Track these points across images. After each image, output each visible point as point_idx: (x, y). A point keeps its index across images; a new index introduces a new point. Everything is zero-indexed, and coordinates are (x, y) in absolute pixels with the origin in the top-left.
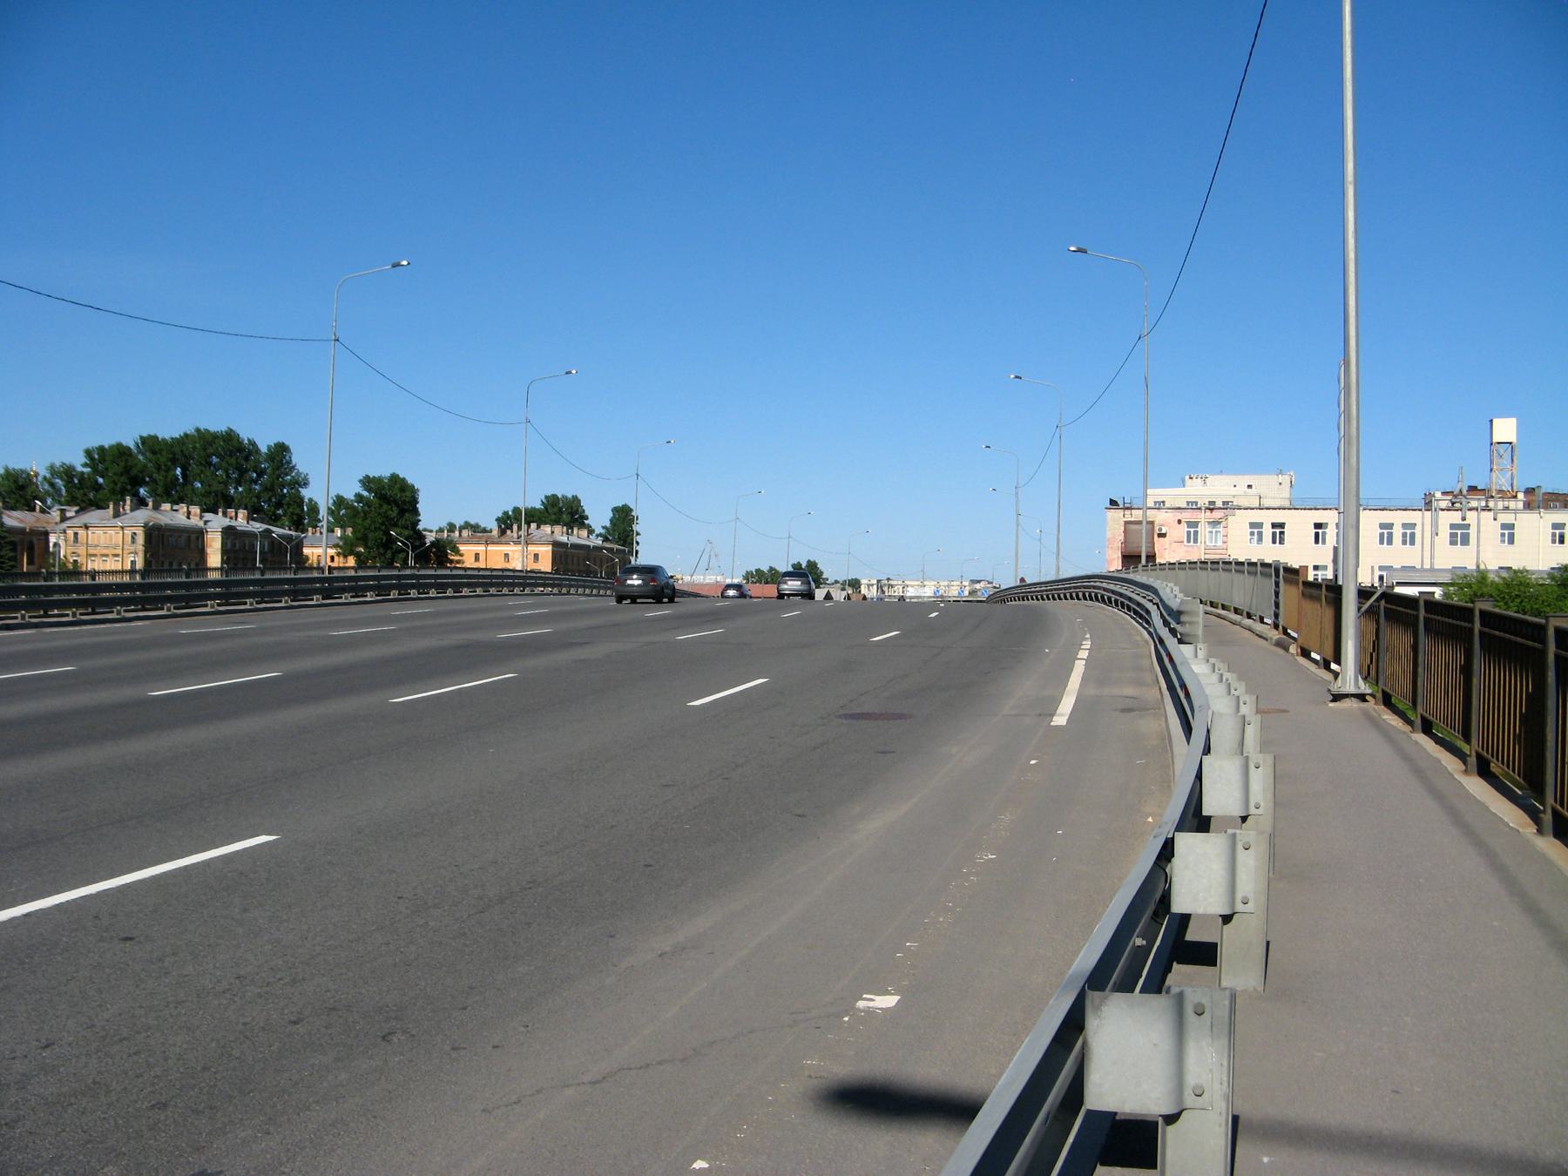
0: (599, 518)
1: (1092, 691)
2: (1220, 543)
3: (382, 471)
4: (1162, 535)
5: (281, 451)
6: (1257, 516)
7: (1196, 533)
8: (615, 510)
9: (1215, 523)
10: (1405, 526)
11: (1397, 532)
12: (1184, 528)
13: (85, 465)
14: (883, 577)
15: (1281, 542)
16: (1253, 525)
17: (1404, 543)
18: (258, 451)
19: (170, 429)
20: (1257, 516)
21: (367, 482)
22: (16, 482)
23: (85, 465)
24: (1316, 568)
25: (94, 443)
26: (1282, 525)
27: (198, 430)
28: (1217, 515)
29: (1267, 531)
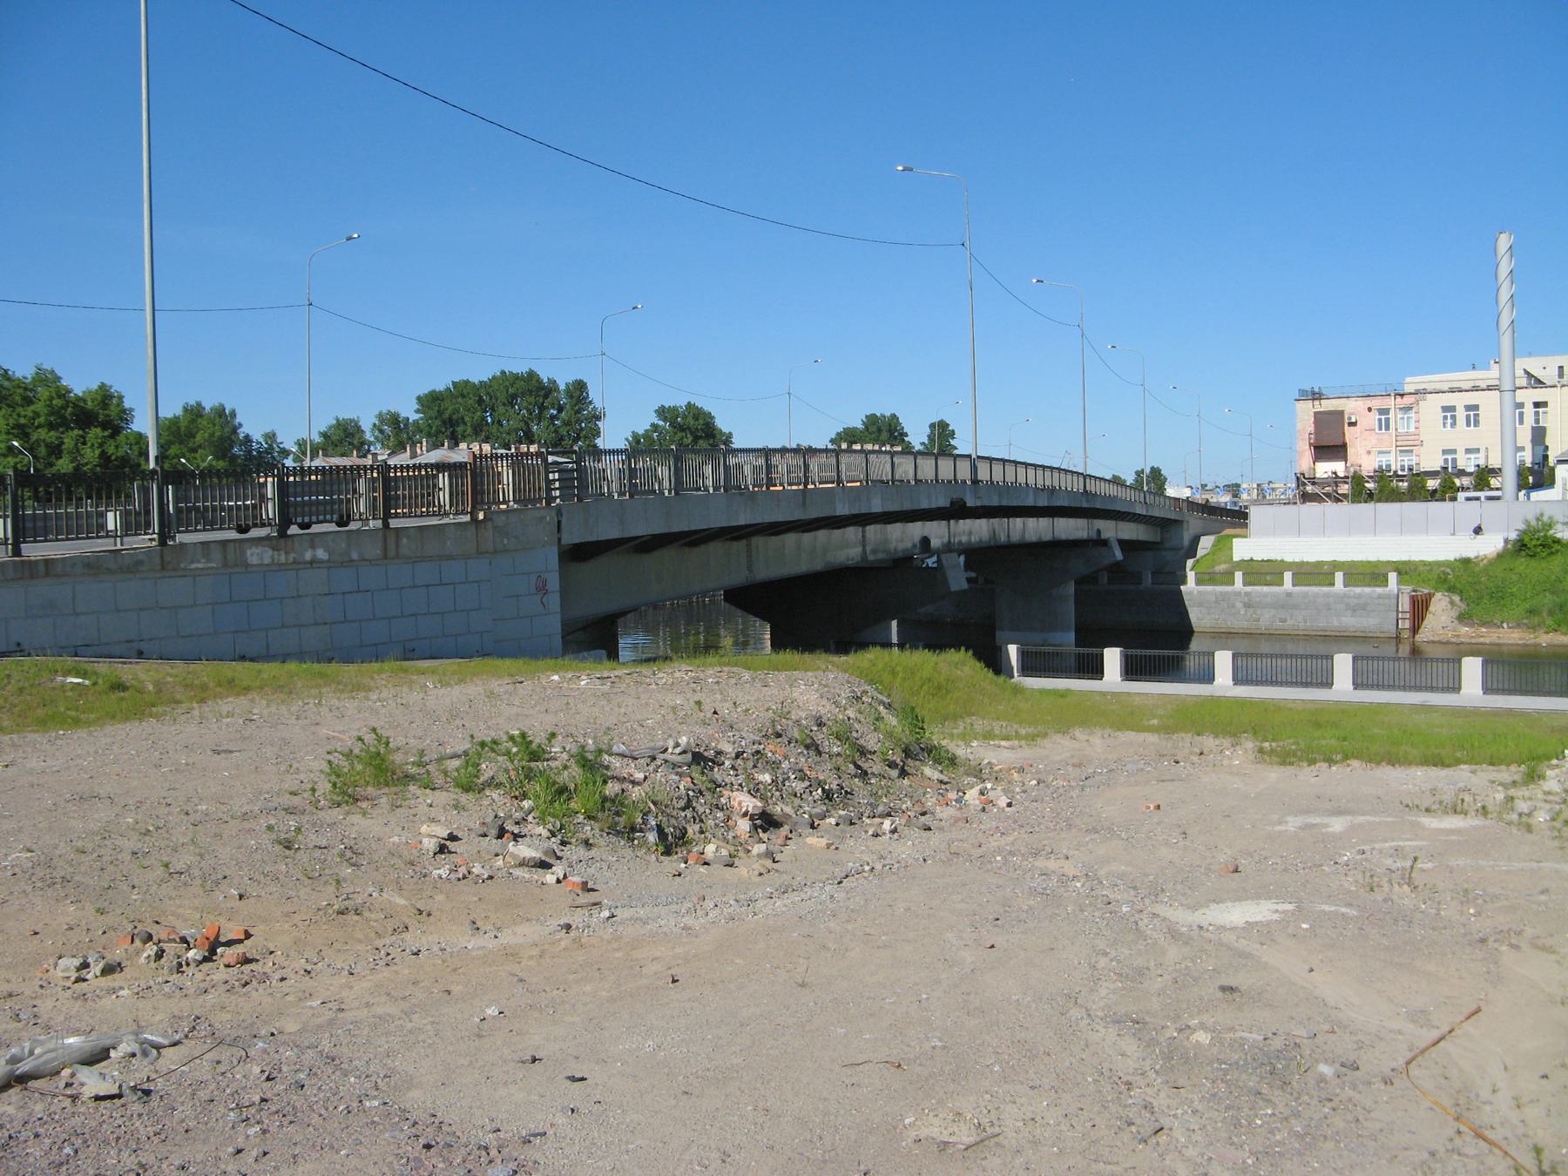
0: (917, 436)
1: (832, 647)
2: (1412, 430)
3: (679, 401)
4: (1352, 424)
5: (580, 386)
6: (1449, 399)
7: (1387, 420)
8: (932, 426)
9: (1408, 409)
10: (1468, 408)
11: (1461, 414)
12: (1375, 416)
13: (417, 411)
14: (1264, 481)
15: (1476, 423)
16: (1445, 409)
17: (1468, 424)
18: (557, 389)
19: (480, 373)
20: (1449, 399)
21: (662, 412)
22: (345, 430)
23: (417, 411)
24: (1468, 451)
25: (424, 390)
26: (1476, 407)
27: (503, 372)
28: (1408, 400)
29: (1461, 414)
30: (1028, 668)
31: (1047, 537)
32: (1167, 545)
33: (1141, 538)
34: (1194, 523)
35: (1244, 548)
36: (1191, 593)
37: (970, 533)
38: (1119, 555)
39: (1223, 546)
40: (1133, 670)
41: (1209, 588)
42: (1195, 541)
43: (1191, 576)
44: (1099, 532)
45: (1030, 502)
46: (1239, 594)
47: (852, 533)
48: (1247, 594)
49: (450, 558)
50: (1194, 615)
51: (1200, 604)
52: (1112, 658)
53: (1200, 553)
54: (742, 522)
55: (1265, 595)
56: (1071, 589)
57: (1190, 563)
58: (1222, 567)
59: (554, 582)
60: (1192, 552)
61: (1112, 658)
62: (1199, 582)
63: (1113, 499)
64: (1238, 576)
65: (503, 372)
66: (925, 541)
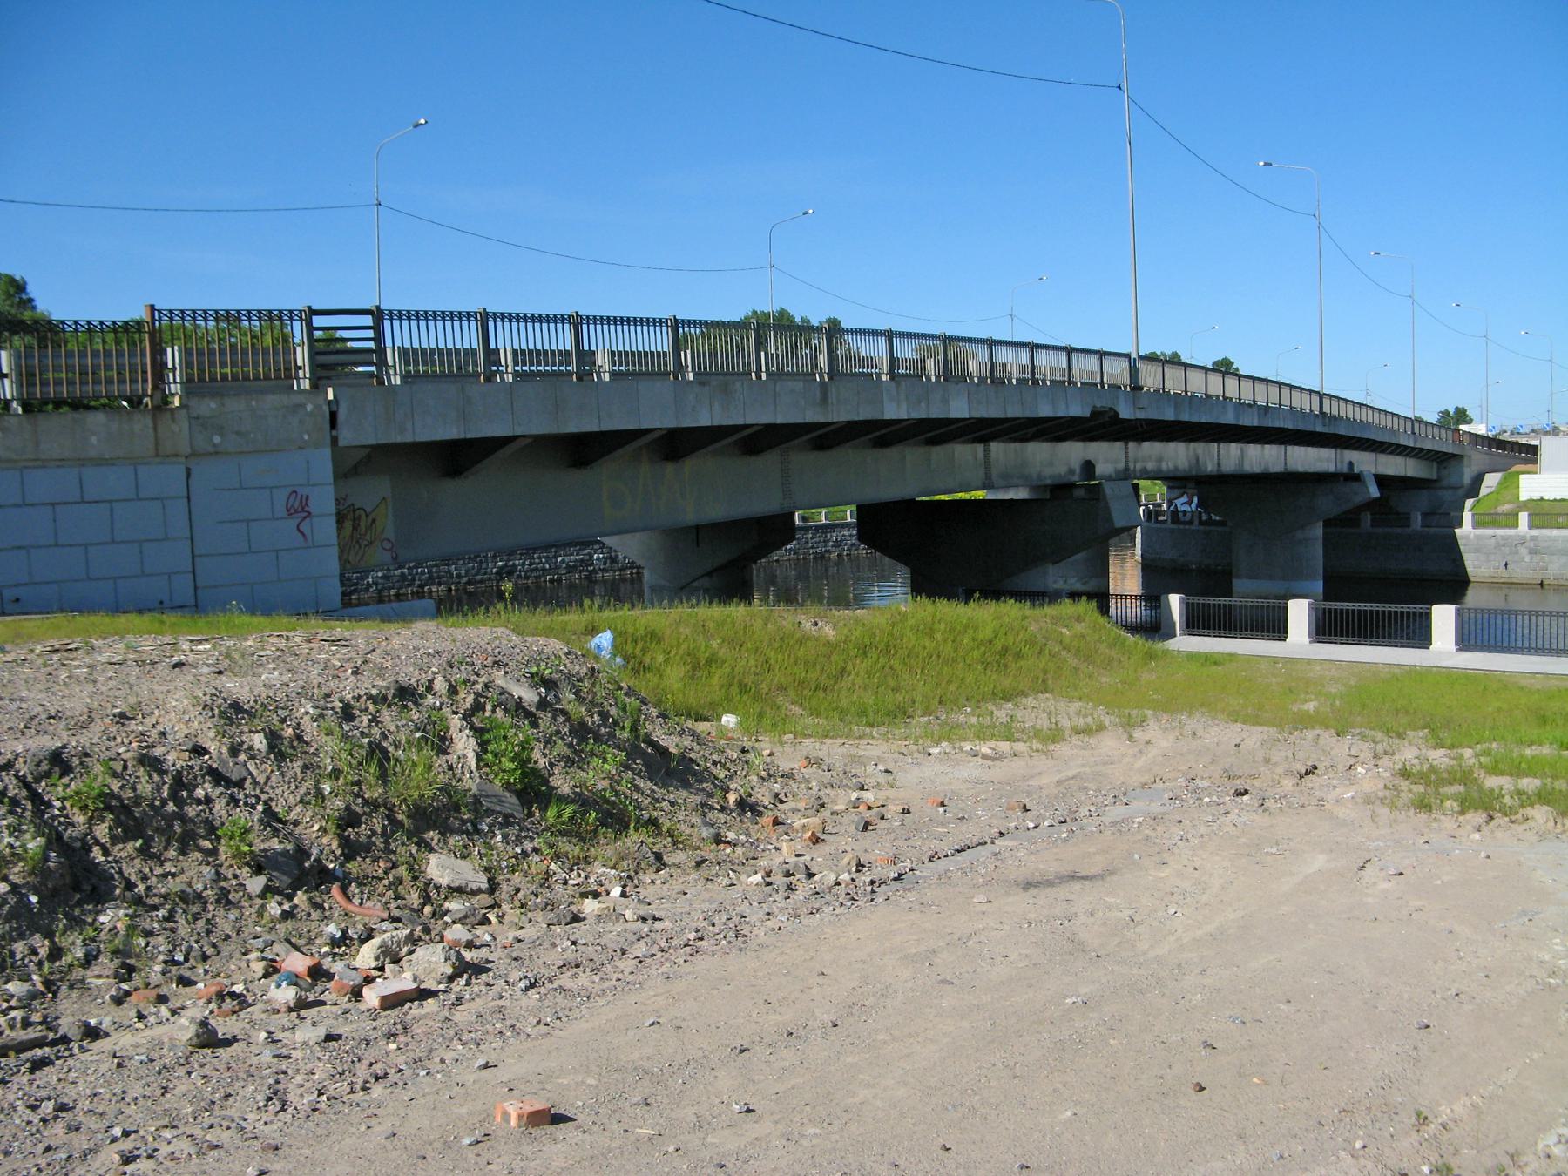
27: (754, 312)
30: (1197, 623)
31: (1277, 467)
32: (1444, 483)
33: (1410, 473)
34: (1477, 458)
35: (1531, 486)
36: (1467, 537)
37: (1160, 460)
38: (1374, 491)
39: (1510, 483)
40: (1327, 628)
41: (1489, 532)
42: (1479, 479)
43: (1467, 517)
44: (1351, 464)
45: (1229, 418)
46: (1522, 541)
47: (965, 453)
48: (1533, 538)
49: (100, 462)
50: (1472, 564)
51: (1478, 550)
52: (1299, 613)
53: (1483, 491)
54: (704, 421)
55: (1555, 539)
56: (1319, 530)
57: (1469, 503)
58: (1506, 508)
59: (324, 501)
60: (1473, 490)
61: (1299, 613)
62: (1476, 525)
63: (1368, 425)
64: (1523, 517)
65: (754, 312)
66: (1088, 467)
